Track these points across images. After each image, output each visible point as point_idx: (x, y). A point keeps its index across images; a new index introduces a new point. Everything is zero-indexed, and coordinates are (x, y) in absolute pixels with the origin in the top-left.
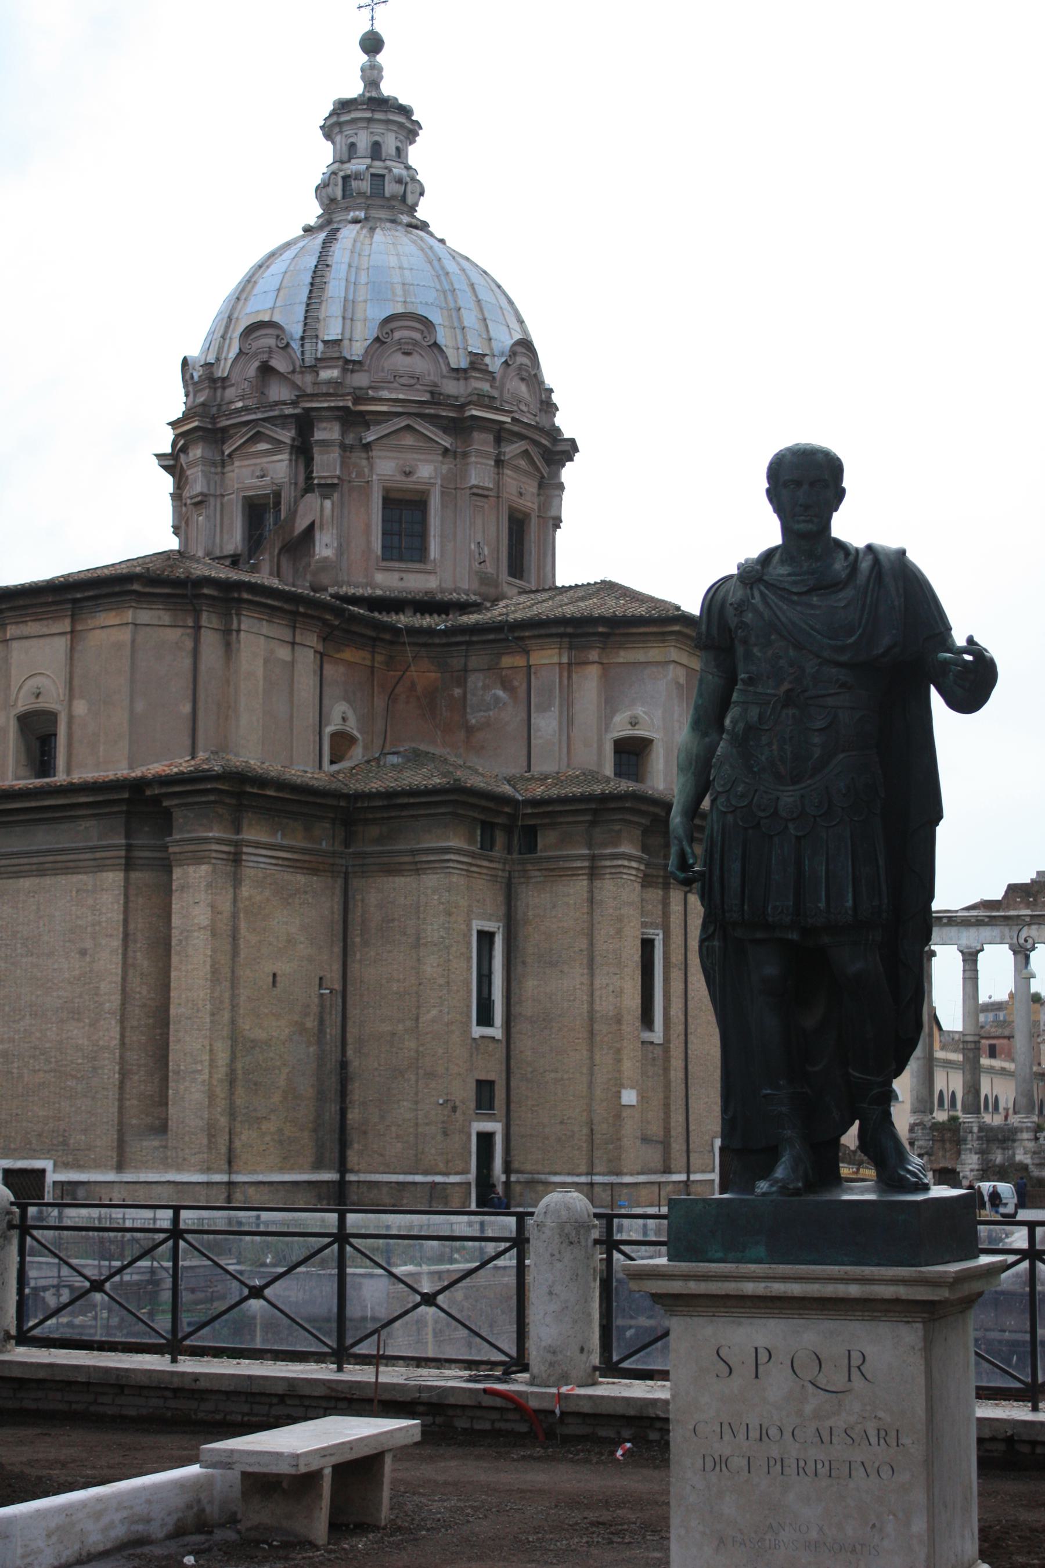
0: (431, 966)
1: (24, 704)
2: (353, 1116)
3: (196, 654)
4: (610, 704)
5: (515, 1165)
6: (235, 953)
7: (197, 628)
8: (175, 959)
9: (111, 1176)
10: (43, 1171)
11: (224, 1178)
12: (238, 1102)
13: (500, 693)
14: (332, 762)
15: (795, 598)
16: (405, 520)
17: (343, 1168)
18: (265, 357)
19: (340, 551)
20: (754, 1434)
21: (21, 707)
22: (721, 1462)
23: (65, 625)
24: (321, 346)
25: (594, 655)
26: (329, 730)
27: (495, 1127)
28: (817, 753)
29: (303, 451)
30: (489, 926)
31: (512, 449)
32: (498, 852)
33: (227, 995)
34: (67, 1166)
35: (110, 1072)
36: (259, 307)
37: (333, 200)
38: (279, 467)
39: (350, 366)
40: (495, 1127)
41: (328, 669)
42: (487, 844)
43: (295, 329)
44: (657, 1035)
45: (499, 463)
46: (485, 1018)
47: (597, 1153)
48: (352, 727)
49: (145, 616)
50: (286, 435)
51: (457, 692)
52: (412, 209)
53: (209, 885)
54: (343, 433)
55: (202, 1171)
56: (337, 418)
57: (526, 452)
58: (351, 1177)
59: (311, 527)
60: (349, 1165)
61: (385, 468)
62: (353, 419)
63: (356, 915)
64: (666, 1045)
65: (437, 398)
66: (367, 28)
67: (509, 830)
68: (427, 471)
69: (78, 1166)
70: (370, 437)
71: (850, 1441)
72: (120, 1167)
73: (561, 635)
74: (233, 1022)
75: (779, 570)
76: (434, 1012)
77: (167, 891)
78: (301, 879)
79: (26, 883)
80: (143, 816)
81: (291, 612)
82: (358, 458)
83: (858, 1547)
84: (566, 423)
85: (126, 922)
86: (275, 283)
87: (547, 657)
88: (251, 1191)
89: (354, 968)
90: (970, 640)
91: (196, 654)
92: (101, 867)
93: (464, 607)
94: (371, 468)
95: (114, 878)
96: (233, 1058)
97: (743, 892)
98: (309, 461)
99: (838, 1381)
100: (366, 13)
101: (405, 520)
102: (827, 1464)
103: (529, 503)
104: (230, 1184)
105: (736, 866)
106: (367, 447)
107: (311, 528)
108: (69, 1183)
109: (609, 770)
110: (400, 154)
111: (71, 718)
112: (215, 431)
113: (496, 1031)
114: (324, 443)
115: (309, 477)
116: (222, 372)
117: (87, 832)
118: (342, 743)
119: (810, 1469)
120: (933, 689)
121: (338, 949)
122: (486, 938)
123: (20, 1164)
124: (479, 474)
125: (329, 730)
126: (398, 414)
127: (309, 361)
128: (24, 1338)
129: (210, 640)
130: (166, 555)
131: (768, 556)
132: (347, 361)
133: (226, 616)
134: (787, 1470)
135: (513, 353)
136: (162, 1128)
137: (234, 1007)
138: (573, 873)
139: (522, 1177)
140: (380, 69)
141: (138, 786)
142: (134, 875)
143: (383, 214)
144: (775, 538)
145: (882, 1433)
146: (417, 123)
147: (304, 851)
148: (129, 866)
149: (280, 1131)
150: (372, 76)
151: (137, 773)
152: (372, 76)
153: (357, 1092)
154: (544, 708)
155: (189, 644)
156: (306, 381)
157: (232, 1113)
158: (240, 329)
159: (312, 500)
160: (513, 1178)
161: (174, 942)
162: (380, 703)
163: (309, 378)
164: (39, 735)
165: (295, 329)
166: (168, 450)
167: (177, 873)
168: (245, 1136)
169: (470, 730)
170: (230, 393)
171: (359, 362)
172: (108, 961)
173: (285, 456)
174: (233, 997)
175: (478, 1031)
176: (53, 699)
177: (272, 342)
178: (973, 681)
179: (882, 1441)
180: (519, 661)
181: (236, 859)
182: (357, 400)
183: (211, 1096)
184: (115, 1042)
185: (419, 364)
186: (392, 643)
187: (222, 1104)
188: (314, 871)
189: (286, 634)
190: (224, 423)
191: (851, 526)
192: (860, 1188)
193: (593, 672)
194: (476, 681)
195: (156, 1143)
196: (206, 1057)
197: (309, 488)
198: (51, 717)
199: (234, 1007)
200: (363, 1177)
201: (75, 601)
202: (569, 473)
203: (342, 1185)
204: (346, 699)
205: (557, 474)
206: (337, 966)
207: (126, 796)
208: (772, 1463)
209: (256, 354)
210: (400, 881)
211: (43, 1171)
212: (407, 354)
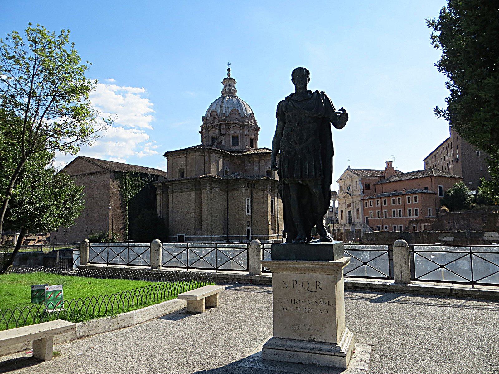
7: (205, 155)
8: (202, 204)
11: (210, 236)
14: (225, 175)
15: (299, 102)
17: (228, 235)
19: (226, 144)
20: (293, 302)
21: (179, 168)
22: (285, 308)
25: (263, 158)
26: (224, 170)
27: (250, 228)
28: (305, 137)
36: (213, 108)
38: (217, 132)
40: (250, 228)
41: (224, 161)
42: (248, 186)
44: (274, 214)
45: (249, 131)
46: (248, 212)
48: (228, 170)
50: (218, 127)
52: (235, 94)
54: (226, 126)
56: (224, 125)
59: (221, 141)
62: (226, 124)
63: (229, 198)
70: (230, 127)
71: (317, 304)
75: (295, 97)
82: (228, 130)
83: (319, 330)
85: (195, 199)
90: (342, 109)
92: (191, 191)
97: (288, 171)
98: (221, 131)
99: (314, 289)
102: (311, 309)
103: (253, 136)
104: (211, 237)
105: (286, 166)
106: (229, 129)
107: (221, 141)
111: (186, 169)
113: (250, 214)
115: (221, 133)
116: (208, 118)
119: (307, 311)
120: (331, 123)
121: (226, 202)
125: (224, 170)
128: (162, 266)
129: (207, 158)
130: (201, 145)
131: (292, 95)
133: (209, 154)
134: (301, 311)
135: (250, 115)
136: (201, 229)
142: (196, 192)
144: (294, 91)
145: (325, 302)
148: (195, 191)
150: (229, 75)
151: (196, 177)
152: (229, 75)
167: (202, 191)
168: (213, 230)
170: (209, 121)
175: (247, 214)
178: (341, 119)
179: (325, 304)
182: (228, 122)
185: (237, 116)
187: (210, 225)
191: (311, 87)
192: (315, 242)
193: (263, 161)
197: (221, 135)
200: (230, 236)
202: (259, 132)
208: (298, 309)
210: (235, 192)
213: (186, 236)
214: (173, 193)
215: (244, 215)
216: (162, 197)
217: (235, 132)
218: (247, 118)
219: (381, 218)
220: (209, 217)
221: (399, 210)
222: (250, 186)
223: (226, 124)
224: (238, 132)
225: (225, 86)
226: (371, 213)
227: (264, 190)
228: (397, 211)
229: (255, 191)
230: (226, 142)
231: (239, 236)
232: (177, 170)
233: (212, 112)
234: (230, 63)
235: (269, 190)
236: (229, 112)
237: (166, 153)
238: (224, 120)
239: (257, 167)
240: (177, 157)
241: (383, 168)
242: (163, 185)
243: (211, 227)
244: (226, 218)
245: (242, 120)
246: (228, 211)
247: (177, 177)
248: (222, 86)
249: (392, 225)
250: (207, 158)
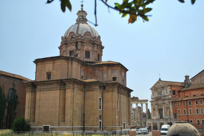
0: (95, 102)
1: (47, 71)
2: (85, 119)
3: (68, 65)
4: (112, 73)
5: (103, 125)
6: (73, 100)
9: (58, 127)
10: (49, 126)
11: (72, 127)
12: (74, 118)
13: (100, 72)
16: (88, 54)
17: (84, 126)
18: (72, 36)
19: (81, 56)
23: (53, 62)
24: (78, 35)
25: (110, 68)
29: (76, 46)
30: (101, 98)
31: (98, 47)
32: (101, 89)
33: (72, 105)
34: (52, 126)
35: (57, 114)
36: (71, 31)
37: (78, 21)
38: (74, 47)
39: (82, 37)
42: (100, 88)
43: (75, 32)
46: (100, 108)
47: (113, 124)
48: (83, 75)
49: (62, 61)
50: (75, 44)
51: (94, 72)
53: (71, 92)
54: (81, 44)
55: (70, 126)
57: (99, 47)
58: (85, 127)
59: (77, 54)
60: (85, 125)
61: (86, 48)
62: (82, 42)
63: (85, 96)
64: (119, 111)
65: (91, 41)
66: (82, 4)
67: (102, 87)
68: (90, 48)
69: (53, 126)
70: (84, 44)
72: (59, 126)
73: (107, 66)
74: (73, 108)
76: (95, 107)
77: (65, 93)
78: (80, 92)
79: (47, 92)
80: (62, 84)
81: (78, 61)
82: (83, 47)
84: (103, 45)
85: (60, 96)
86: (73, 28)
87: (105, 68)
88: (75, 128)
89: (85, 102)
91: (68, 65)
92: (57, 90)
93: (94, 63)
94: (84, 48)
95: (58, 91)
96: (73, 112)
100: (81, 3)
101: (88, 54)
103: (100, 53)
106: (84, 46)
107: (77, 54)
108: (52, 128)
109: (112, 80)
110: (85, 17)
111: (53, 73)
112: (66, 44)
113: (101, 110)
114: (79, 45)
116: (67, 37)
117: (55, 85)
118: (82, 77)
122: (100, 99)
123: (46, 126)
124: (95, 49)
125: (81, 75)
126: (87, 42)
127: (77, 36)
129: (70, 64)
132: (81, 36)
133: (71, 61)
135: (98, 37)
136: (64, 121)
137: (73, 106)
138: (110, 92)
139: (104, 127)
140: (83, 8)
141: (62, 80)
142: (61, 91)
143: (84, 22)
146: (87, 14)
147: (80, 88)
148: (60, 90)
149: (78, 121)
150: (82, 9)
151: (62, 79)
152: (82, 9)
153: (86, 117)
154: (105, 74)
155: (67, 64)
156: (77, 38)
157: (73, 119)
158: (69, 33)
159: (78, 51)
160: (103, 127)
161: (66, 99)
162: (86, 73)
163: (77, 38)
164: (49, 75)
165: (75, 32)
166: (59, 46)
167: (66, 90)
168: (74, 122)
169: (96, 76)
170: (68, 40)
171: (83, 36)
172: (58, 101)
173: (74, 46)
174: (73, 105)
175: (100, 110)
176: (51, 70)
177: (73, 34)
180: (102, 68)
181: (74, 89)
183: (71, 117)
184: (58, 111)
185: (89, 37)
186: (87, 66)
187: (72, 118)
188: (81, 91)
190: (67, 43)
193: (110, 70)
194: (96, 71)
195: (63, 123)
196: (70, 112)
197: (77, 49)
198: (51, 72)
199: (73, 106)
201: (54, 59)
203: (84, 128)
204: (83, 72)
205: (102, 50)
206: (83, 102)
207: (60, 81)
209: (71, 35)
210: (91, 92)
211: (49, 126)
212: (88, 36)
213: (51, 127)
214: (40, 91)
215: (98, 110)
216: (30, 95)
218: (96, 38)
219: (186, 114)
220: (72, 111)
221: (201, 108)
222: (101, 88)
226: (190, 110)
227: (112, 92)
228: (200, 109)
229: (105, 91)
231: (94, 127)
233: (70, 33)
234: (83, 1)
235: (116, 91)
237: (36, 60)
238: (80, 39)
239: (106, 74)
240: (46, 63)
242: (32, 85)
244: (83, 112)
246: (85, 107)
247: (45, 78)
249: (196, 119)
250: (70, 64)
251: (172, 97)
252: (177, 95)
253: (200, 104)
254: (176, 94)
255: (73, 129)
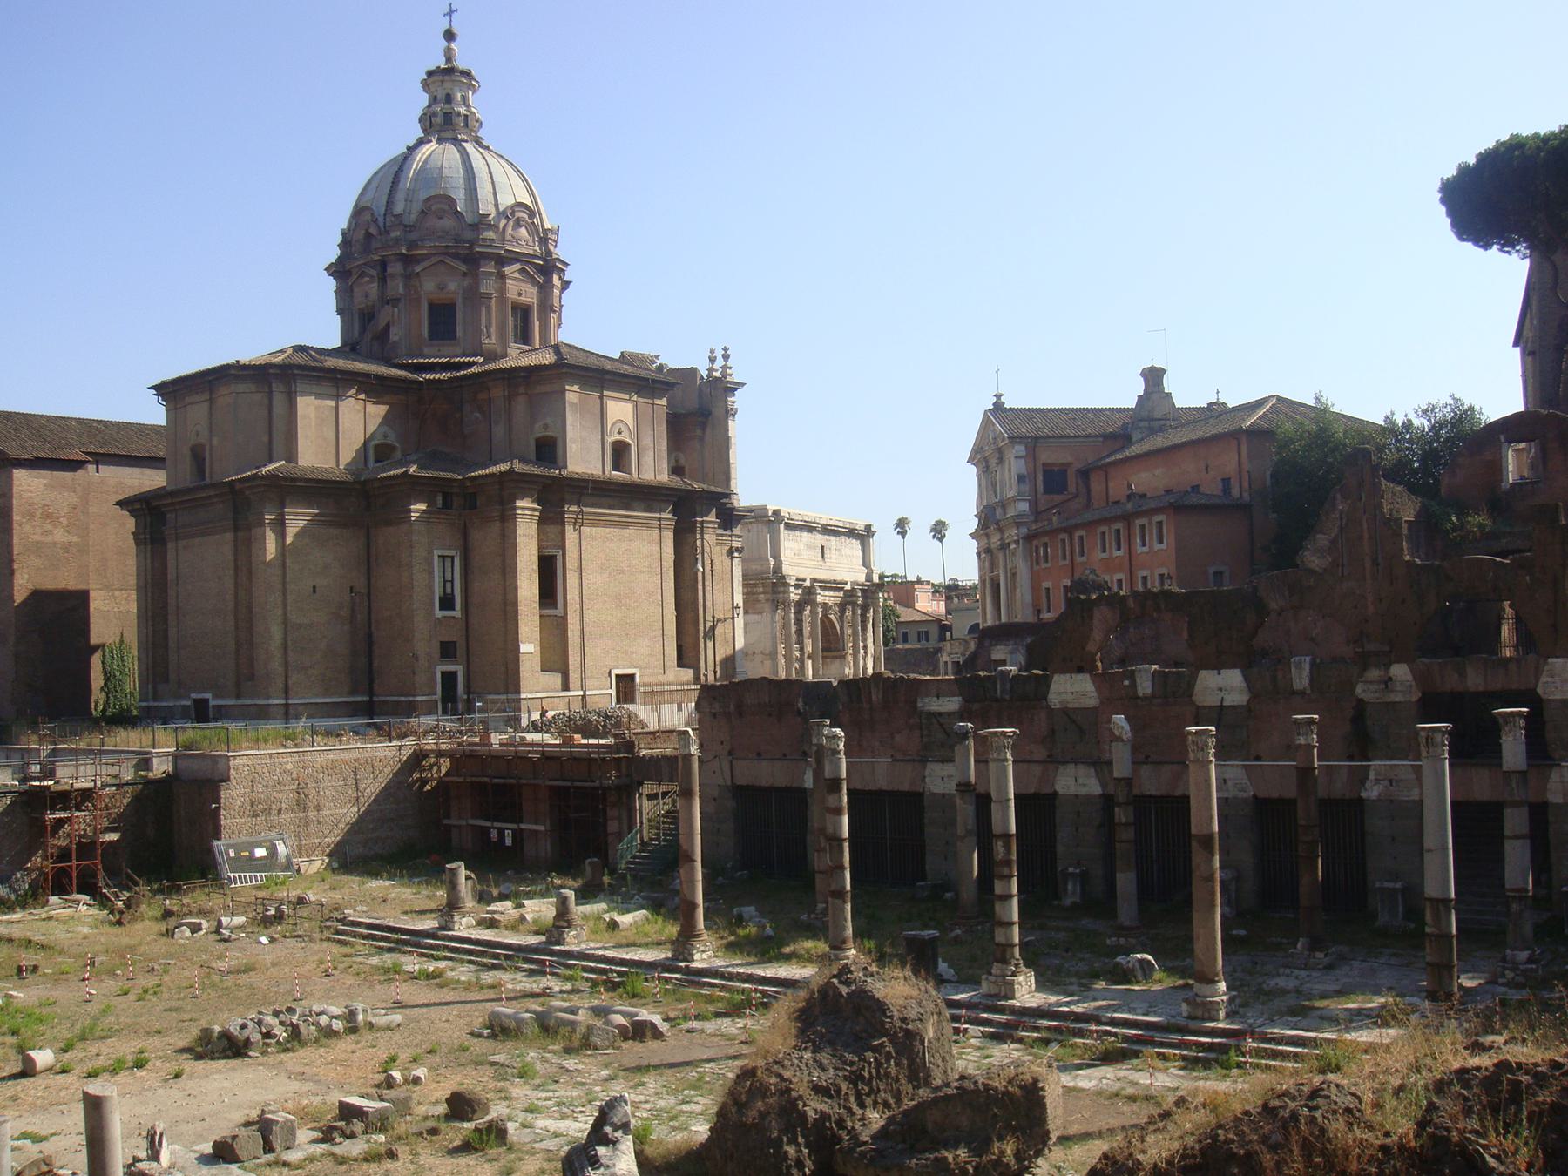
2: (375, 664)
7: (271, 392)
14: (377, 461)
17: (371, 694)
26: (610, 439)
27: (459, 669)
38: (373, 289)
39: (409, 228)
50: (373, 272)
59: (388, 325)
62: (408, 260)
70: (418, 269)
74: (285, 614)
79: (197, 540)
85: (236, 560)
104: (287, 705)
107: (388, 325)
137: (285, 605)
155: (266, 401)
168: (293, 678)
185: (448, 223)
189: (333, 391)
198: (203, 447)
199: (285, 605)
217: (442, 288)
223: (408, 260)
224: (452, 286)
225: (434, 100)
230: (406, 325)
232: (186, 451)
236: (416, 207)
240: (188, 400)
241: (1131, 403)
243: (286, 665)
245: (468, 235)
248: (424, 99)
251: (1041, 508)
252: (1076, 496)
253: (1157, 547)
254: (1072, 488)
255: (291, 711)
